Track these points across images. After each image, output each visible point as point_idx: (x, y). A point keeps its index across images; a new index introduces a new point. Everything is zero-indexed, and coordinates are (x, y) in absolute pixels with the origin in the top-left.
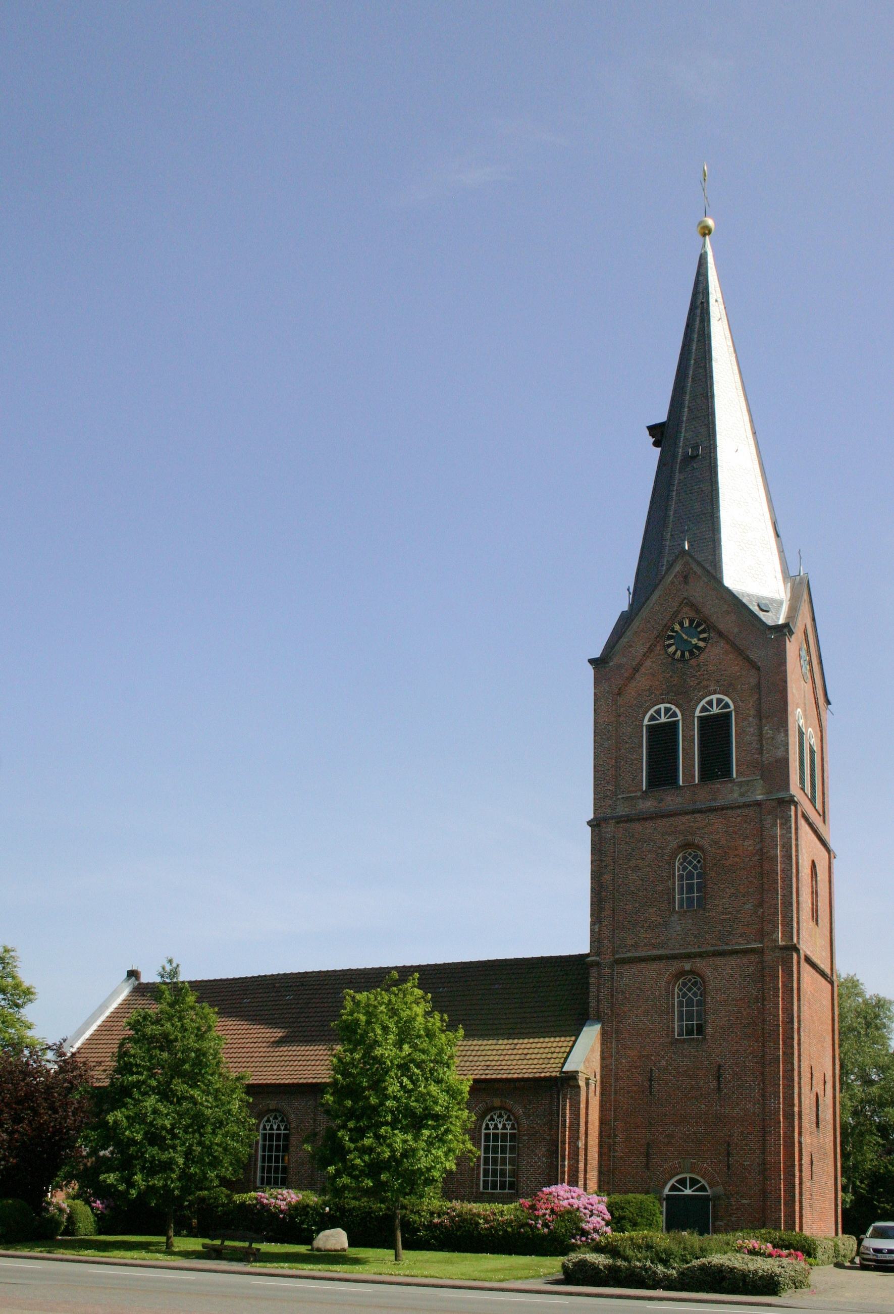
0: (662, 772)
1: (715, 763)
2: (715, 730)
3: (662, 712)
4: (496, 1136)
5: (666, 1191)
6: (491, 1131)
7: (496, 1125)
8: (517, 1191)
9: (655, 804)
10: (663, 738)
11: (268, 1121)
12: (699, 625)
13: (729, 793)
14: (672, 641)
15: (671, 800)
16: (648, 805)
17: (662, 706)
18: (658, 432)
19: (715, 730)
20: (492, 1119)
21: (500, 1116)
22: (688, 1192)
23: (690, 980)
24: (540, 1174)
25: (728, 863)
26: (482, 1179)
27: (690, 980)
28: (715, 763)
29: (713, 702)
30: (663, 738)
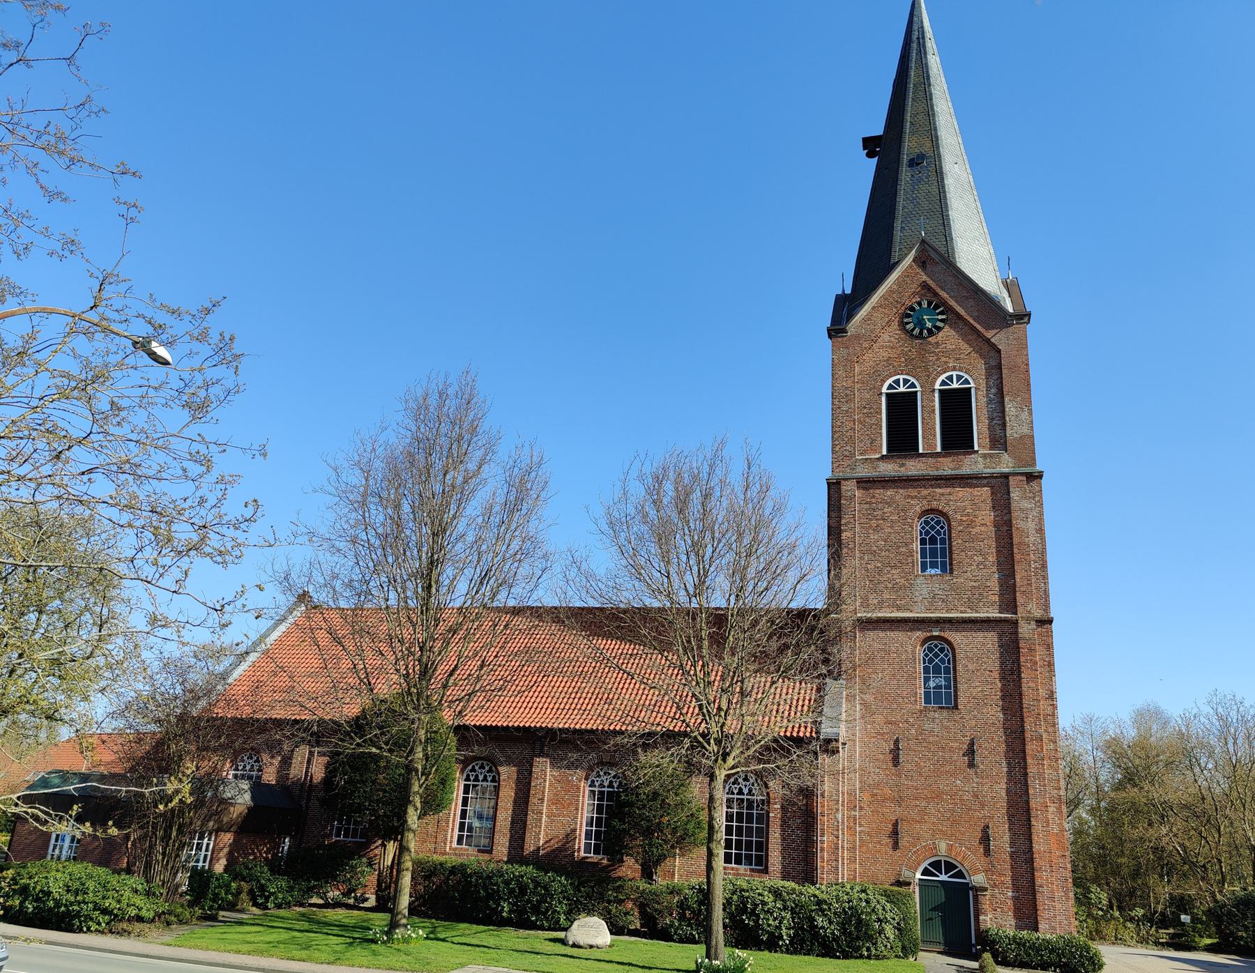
0: (902, 438)
1: (957, 435)
2: (956, 405)
3: (900, 382)
4: (750, 803)
5: (918, 876)
6: (745, 797)
7: (740, 789)
8: (767, 867)
9: (897, 468)
10: (902, 410)
11: (473, 770)
12: (936, 307)
13: (972, 464)
14: (910, 320)
15: (913, 467)
16: (889, 469)
17: (901, 377)
18: (871, 145)
19: (956, 405)
20: (473, 770)
21: (482, 767)
22: (943, 877)
23: (936, 646)
24: (794, 849)
25: (974, 531)
26: (583, 841)
27: (936, 646)
28: (957, 435)
29: (949, 378)
30: (902, 410)
